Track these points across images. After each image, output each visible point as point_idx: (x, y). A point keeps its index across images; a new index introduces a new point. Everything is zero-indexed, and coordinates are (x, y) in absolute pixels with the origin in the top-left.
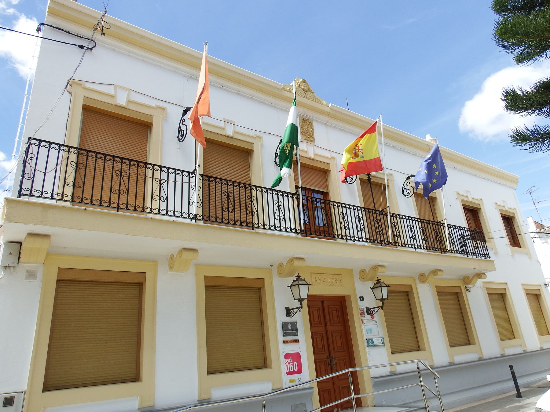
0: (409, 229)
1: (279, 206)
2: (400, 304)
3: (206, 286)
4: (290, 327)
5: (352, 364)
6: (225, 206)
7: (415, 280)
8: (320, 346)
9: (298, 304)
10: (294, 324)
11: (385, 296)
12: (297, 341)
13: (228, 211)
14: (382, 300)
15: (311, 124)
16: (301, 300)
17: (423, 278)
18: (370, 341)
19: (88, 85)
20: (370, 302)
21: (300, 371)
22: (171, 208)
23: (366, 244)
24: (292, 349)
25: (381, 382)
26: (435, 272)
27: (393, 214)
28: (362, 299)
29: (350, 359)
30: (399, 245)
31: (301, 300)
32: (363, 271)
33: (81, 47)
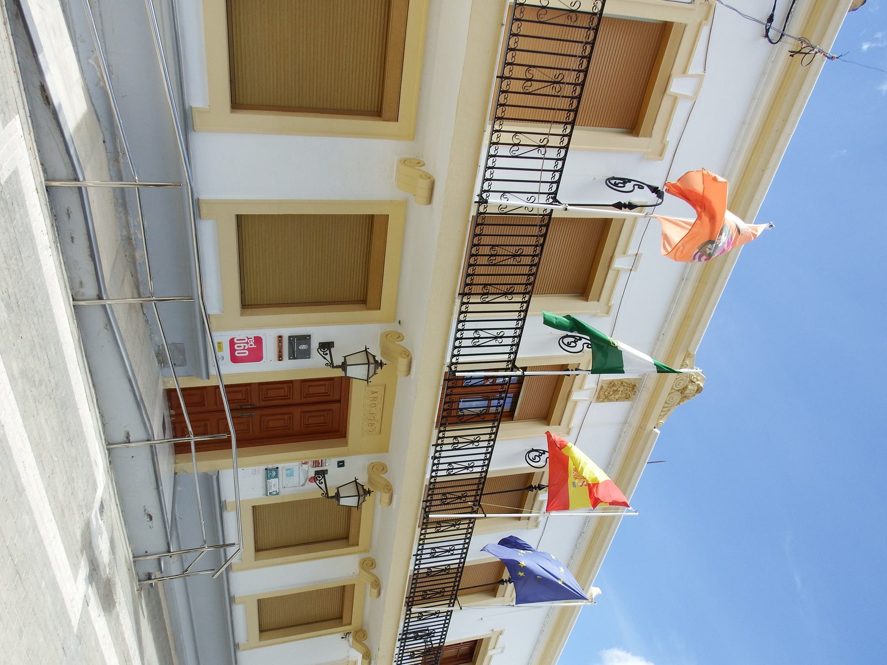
0: (448, 548)
1: (496, 338)
2: (328, 524)
3: (372, 217)
4: (303, 347)
5: (241, 443)
6: (499, 251)
7: (366, 551)
8: (271, 393)
9: (338, 361)
10: (306, 354)
11: (344, 502)
12: (280, 358)
13: (492, 255)
14: (337, 496)
15: (627, 398)
16: (344, 366)
17: (368, 564)
18: (274, 473)
19: (705, 30)
20: (336, 478)
21: (235, 359)
22: (500, 162)
23: (428, 476)
24: (269, 349)
25: (211, 483)
26: (377, 585)
27: (473, 523)
28: (341, 464)
29: (254, 438)
30: (440, 432)
31: (344, 366)
32: (384, 468)
33: (771, 19)
